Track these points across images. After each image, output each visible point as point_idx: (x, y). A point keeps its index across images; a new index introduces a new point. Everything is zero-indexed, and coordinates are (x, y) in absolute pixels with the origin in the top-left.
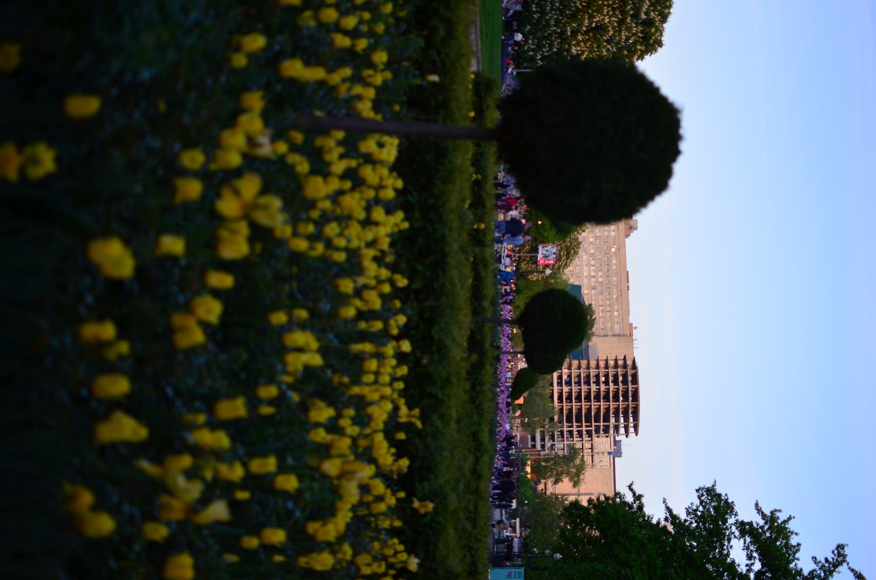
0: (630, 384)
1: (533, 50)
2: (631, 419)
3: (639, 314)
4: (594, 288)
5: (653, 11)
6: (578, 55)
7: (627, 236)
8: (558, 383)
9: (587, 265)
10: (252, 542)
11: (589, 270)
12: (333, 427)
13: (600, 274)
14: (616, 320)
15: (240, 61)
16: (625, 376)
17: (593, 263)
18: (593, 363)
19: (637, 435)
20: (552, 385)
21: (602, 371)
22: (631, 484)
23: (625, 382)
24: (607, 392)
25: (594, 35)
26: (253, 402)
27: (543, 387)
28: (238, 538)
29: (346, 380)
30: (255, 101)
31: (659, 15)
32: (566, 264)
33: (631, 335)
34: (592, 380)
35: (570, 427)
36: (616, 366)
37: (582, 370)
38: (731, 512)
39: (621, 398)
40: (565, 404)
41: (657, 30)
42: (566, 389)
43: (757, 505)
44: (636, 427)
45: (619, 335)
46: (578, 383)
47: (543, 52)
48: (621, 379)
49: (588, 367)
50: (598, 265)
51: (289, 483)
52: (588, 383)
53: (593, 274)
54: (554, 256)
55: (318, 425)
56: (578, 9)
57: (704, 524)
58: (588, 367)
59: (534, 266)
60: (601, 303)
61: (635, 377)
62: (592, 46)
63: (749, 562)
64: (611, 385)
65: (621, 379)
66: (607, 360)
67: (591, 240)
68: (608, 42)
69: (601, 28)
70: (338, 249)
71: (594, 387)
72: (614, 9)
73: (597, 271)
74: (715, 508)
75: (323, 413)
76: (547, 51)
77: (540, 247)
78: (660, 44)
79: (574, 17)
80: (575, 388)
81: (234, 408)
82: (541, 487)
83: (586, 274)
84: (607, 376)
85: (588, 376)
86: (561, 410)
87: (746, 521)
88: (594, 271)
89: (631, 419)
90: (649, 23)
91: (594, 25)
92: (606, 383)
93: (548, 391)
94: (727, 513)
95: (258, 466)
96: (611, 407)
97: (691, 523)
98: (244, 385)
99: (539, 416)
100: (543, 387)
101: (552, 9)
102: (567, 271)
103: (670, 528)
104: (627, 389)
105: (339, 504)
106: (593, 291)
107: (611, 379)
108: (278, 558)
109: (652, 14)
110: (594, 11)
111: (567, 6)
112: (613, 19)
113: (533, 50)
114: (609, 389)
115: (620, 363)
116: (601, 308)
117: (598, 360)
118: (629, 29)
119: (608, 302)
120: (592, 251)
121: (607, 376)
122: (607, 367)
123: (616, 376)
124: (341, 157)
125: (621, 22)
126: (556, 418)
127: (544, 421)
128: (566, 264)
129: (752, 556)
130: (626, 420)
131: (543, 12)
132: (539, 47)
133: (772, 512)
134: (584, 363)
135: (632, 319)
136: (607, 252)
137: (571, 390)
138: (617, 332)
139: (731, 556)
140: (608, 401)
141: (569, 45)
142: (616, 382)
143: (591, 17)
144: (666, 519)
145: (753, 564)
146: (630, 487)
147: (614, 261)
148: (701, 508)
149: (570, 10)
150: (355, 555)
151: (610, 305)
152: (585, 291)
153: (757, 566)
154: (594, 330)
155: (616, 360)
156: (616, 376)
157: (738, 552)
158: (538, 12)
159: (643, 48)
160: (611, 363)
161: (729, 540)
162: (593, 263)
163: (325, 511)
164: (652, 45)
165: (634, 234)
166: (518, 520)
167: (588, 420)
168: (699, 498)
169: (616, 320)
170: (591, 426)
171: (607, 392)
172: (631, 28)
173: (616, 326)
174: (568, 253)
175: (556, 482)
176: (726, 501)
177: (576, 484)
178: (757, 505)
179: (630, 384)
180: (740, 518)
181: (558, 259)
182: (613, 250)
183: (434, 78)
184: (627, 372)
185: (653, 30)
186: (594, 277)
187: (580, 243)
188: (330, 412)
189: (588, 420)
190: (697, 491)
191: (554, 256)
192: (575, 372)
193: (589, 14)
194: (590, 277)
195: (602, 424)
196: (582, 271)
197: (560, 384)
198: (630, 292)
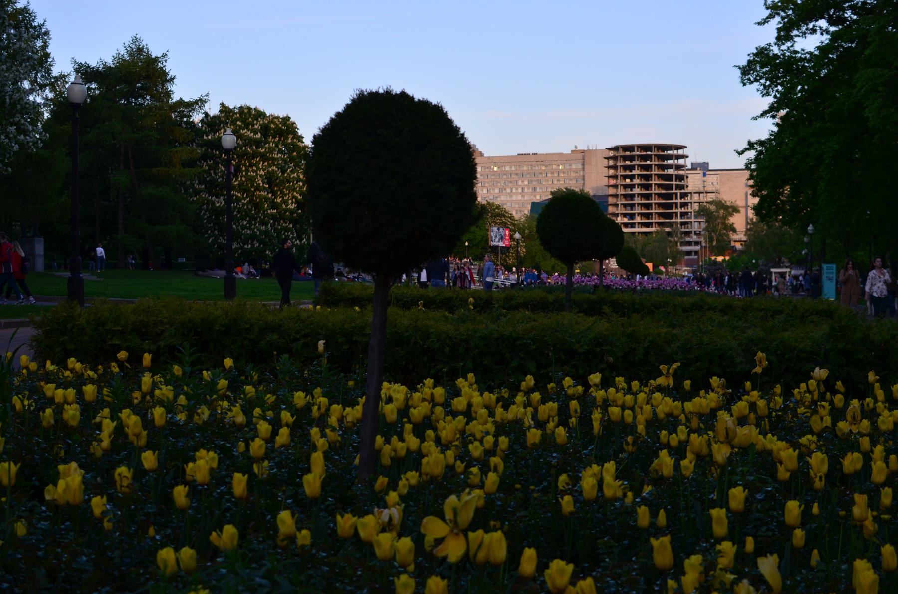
0: (633, 153)
2: (670, 152)
3: (562, 144)
4: (535, 189)
5: (253, 125)
6: (297, 202)
8: (632, 227)
9: (511, 197)
10: (799, 535)
11: (516, 194)
12: (679, 452)
13: (520, 183)
14: (567, 167)
15: (304, 537)
16: (625, 158)
17: (508, 190)
18: (612, 191)
19: (686, 147)
20: (633, 233)
21: (620, 182)
22: (737, 152)
23: (631, 158)
24: (641, 177)
25: (277, 186)
26: (657, 532)
27: (635, 242)
28: (794, 550)
29: (630, 439)
30: (345, 522)
31: (257, 120)
32: (510, 218)
33: (583, 152)
34: (629, 192)
35: (677, 216)
36: (615, 167)
38: (766, 49)
39: (648, 163)
40: (653, 221)
42: (638, 219)
43: (759, 24)
44: (678, 148)
45: (583, 165)
46: (632, 206)
48: (628, 163)
49: (616, 196)
50: (511, 185)
51: (738, 495)
52: (632, 197)
53: (520, 190)
54: (501, 230)
55: (677, 467)
57: (779, 78)
59: (512, 251)
60: (550, 183)
61: (627, 148)
63: (819, 32)
64: (634, 172)
65: (628, 163)
66: (609, 177)
69: (270, 179)
70: (496, 444)
71: (636, 191)
72: (251, 166)
73: (517, 186)
74: (762, 66)
75: (665, 462)
76: (293, 233)
77: (492, 244)
79: (258, 207)
80: (637, 210)
81: (662, 549)
82: (738, 246)
83: (520, 198)
84: (625, 177)
85: (625, 196)
86: (659, 224)
87: (776, 35)
89: (670, 152)
90: (265, 129)
92: (632, 177)
94: (768, 54)
95: (720, 529)
97: (777, 91)
98: (638, 539)
103: (783, 112)
104: (638, 156)
105: (759, 447)
106: (538, 190)
107: (628, 173)
108: (815, 509)
110: (253, 186)
114: (639, 175)
115: (611, 163)
116: (555, 182)
117: (609, 186)
118: (271, 150)
119: (549, 175)
120: (497, 191)
121: (625, 177)
122: (615, 177)
123: (625, 168)
124: (402, 439)
125: (264, 158)
126: (667, 230)
127: (670, 242)
128: (510, 218)
129: (812, 29)
130: (670, 157)
131: (253, 238)
133: (767, 9)
134: (611, 200)
135: (567, 151)
136: (498, 175)
138: (580, 166)
139: (812, 50)
140: (650, 176)
141: (286, 211)
142: (631, 168)
143: (258, 189)
144: (774, 117)
145: (821, 28)
146: (740, 153)
147: (508, 169)
148: (763, 81)
150: (812, 433)
151: (553, 173)
152: (537, 199)
153: (823, 23)
154: (577, 190)
155: (609, 167)
156: (625, 168)
157: (808, 43)
159: (291, 136)
160: (612, 172)
161: (796, 52)
162: (508, 190)
163: (767, 462)
164: (288, 127)
166: (773, 270)
167: (670, 197)
168: (751, 83)
169: (567, 167)
170: (676, 194)
171: (641, 177)
172: (270, 148)
173: (574, 167)
175: (734, 230)
176: (755, 55)
177: (736, 210)
178: (759, 24)
179: (633, 153)
180: (773, 40)
181: (505, 225)
182: (496, 169)
183: (321, 344)
185: (272, 126)
186: (523, 189)
188: (664, 454)
189: (670, 197)
190: (745, 84)
191: (501, 230)
192: (621, 210)
193: (255, 191)
194: (523, 193)
195: (674, 183)
196: (517, 202)
198: (539, 152)
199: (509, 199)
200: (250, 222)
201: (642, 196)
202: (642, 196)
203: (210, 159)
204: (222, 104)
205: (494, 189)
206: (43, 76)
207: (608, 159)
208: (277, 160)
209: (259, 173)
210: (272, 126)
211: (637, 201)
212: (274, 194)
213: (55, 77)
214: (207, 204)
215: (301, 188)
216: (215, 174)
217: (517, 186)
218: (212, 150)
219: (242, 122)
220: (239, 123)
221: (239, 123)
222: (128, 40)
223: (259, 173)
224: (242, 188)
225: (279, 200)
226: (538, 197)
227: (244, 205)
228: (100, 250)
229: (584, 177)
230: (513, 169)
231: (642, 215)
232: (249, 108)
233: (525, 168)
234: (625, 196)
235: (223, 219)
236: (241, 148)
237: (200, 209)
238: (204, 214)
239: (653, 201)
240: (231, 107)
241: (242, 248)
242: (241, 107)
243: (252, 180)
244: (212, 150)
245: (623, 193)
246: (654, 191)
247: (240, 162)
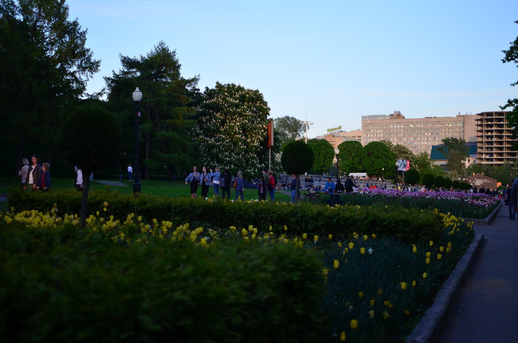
1: (255, 169)
3: (449, 110)
4: (435, 138)
5: (235, 95)
6: (260, 141)
7: (404, 118)
8: (491, 161)
9: (421, 142)
11: (424, 141)
13: (426, 134)
14: (454, 125)
16: (488, 120)
17: (419, 139)
18: (480, 139)
20: (492, 165)
21: (484, 134)
23: (491, 120)
24: (497, 131)
25: (248, 131)
27: (493, 170)
31: (238, 92)
32: (411, 154)
33: (464, 116)
34: (490, 140)
36: (481, 125)
37: (484, 146)
39: (502, 123)
40: (504, 157)
41: (248, 93)
42: (495, 156)
45: (464, 124)
46: (492, 149)
47: (256, 163)
48: (490, 123)
49: (482, 142)
50: (420, 135)
52: (492, 143)
53: (426, 139)
54: (404, 161)
56: (232, 141)
58: (482, 142)
60: (444, 134)
61: (489, 114)
62: (255, 133)
64: (493, 128)
65: (490, 123)
66: (478, 131)
67: (405, 139)
68: (253, 123)
69: (243, 127)
71: (494, 139)
72: (232, 119)
73: (425, 136)
76: (257, 160)
77: (399, 169)
78: (257, 91)
79: (235, 144)
80: (495, 151)
83: (426, 143)
84: (488, 131)
85: (488, 143)
86: (508, 159)
88: (424, 138)
90: (243, 99)
91: (241, 132)
92: (492, 131)
93: (496, 168)
96: (506, 129)
99: (510, 173)
100: (493, 170)
101: (229, 157)
102: (415, 153)
104: (496, 119)
106: (437, 139)
107: (489, 129)
109: (236, 96)
110: (232, 131)
111: (228, 147)
112: (238, 120)
113: (255, 169)
114: (496, 130)
115: (479, 123)
116: (447, 134)
117: (478, 137)
118: (245, 110)
119: (443, 130)
120: (412, 139)
121: (488, 131)
122: (481, 131)
123: (488, 126)
125: (240, 115)
126: (511, 163)
127: (513, 170)
128: (411, 154)
131: (230, 162)
132: (253, 165)
134: (479, 145)
135: (454, 116)
136: (414, 129)
137: (495, 153)
138: (462, 125)
140: (503, 130)
141: (252, 147)
142: (491, 126)
143: (236, 133)
147: (419, 126)
149: (231, 146)
151: (445, 129)
152: (436, 144)
155: (478, 125)
156: (488, 126)
158: (230, 165)
159: (259, 102)
160: (479, 128)
164: (257, 96)
165: (403, 114)
169: (454, 125)
171: (497, 131)
172: (244, 109)
173: (458, 125)
174: (403, 152)
181: (407, 159)
182: (412, 126)
184: (485, 119)
185: (247, 96)
186: (428, 138)
187: (398, 145)
191: (404, 161)
193: (234, 134)
194: (428, 140)
196: (424, 145)
197: (492, 160)
198: (437, 116)
199: (419, 143)
200: (230, 153)
201: (498, 142)
202: (498, 142)
203: (208, 115)
204: (217, 83)
205: (410, 138)
206: (85, 62)
207: (477, 120)
208: (248, 116)
209: (236, 124)
210: (247, 96)
211: (495, 145)
212: (246, 136)
213: (92, 63)
214: (204, 142)
215: (262, 133)
216: (210, 124)
217: (425, 136)
218: (209, 110)
219: (229, 93)
220: (226, 94)
221: (226, 94)
222: (157, 44)
223: (236, 124)
224: (225, 132)
225: (249, 141)
226: (437, 143)
227: (226, 143)
228: (130, 169)
229: (464, 131)
230: (422, 126)
231: (498, 154)
232: (234, 85)
233: (429, 126)
234: (488, 143)
235: (213, 151)
236: (226, 109)
237: (199, 145)
238: (202, 148)
239: (504, 146)
240: (223, 84)
241: (224, 168)
242: (229, 84)
243: (232, 128)
244: (209, 110)
245: (486, 140)
246: (505, 139)
247: (226, 117)
